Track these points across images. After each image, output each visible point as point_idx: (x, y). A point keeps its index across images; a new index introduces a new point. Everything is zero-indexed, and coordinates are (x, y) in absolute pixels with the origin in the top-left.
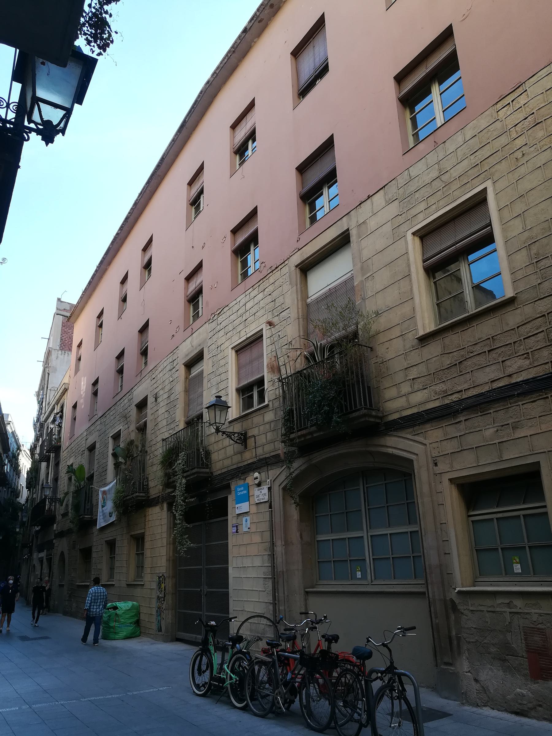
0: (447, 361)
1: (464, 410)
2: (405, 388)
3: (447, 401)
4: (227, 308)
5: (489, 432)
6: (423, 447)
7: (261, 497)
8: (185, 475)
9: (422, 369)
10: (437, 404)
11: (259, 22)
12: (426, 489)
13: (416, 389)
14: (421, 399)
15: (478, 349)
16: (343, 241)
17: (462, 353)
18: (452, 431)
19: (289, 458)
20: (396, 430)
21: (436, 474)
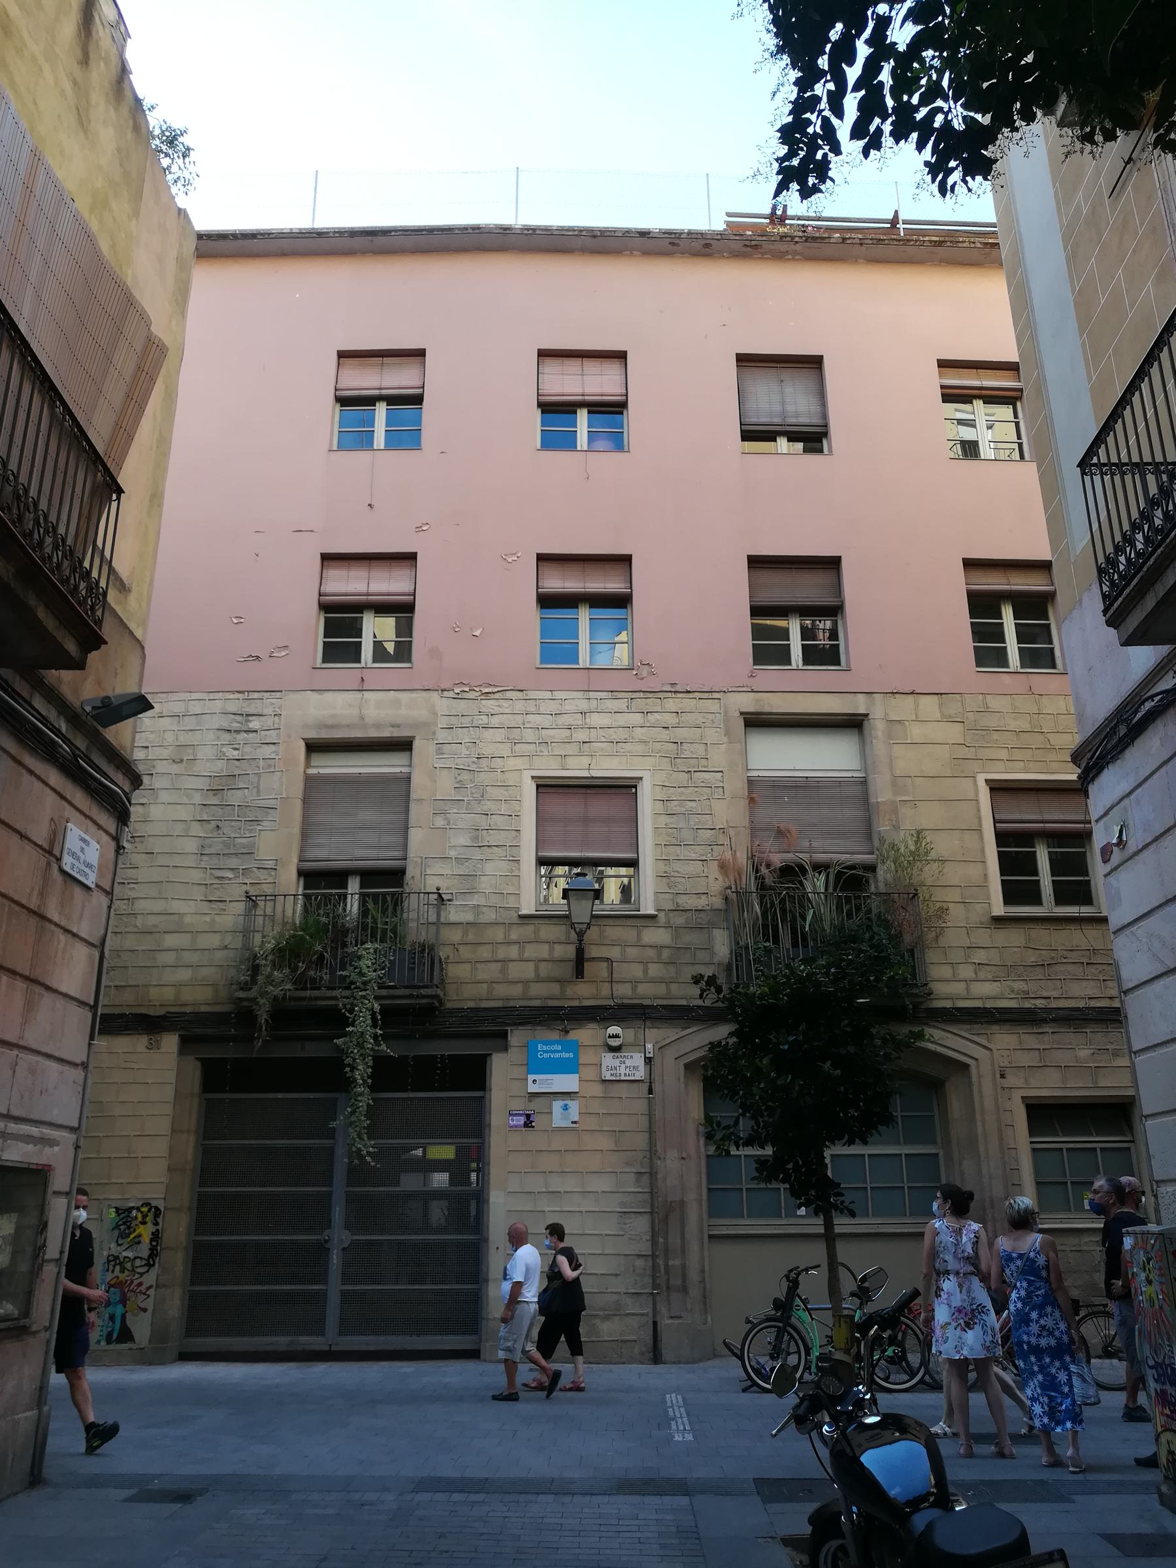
0: (1032, 958)
1: (1054, 1020)
2: (966, 972)
3: (1027, 1005)
4: (520, 695)
5: (1084, 1053)
6: (988, 1052)
7: (622, 1070)
8: (384, 992)
9: (994, 957)
10: (1012, 1004)
11: (672, 244)
12: (989, 1104)
13: (982, 977)
14: (987, 992)
15: (1073, 957)
16: (854, 724)
17: (1053, 954)
18: (1031, 1041)
19: (708, 1017)
20: (944, 1021)
21: (1003, 1089)
